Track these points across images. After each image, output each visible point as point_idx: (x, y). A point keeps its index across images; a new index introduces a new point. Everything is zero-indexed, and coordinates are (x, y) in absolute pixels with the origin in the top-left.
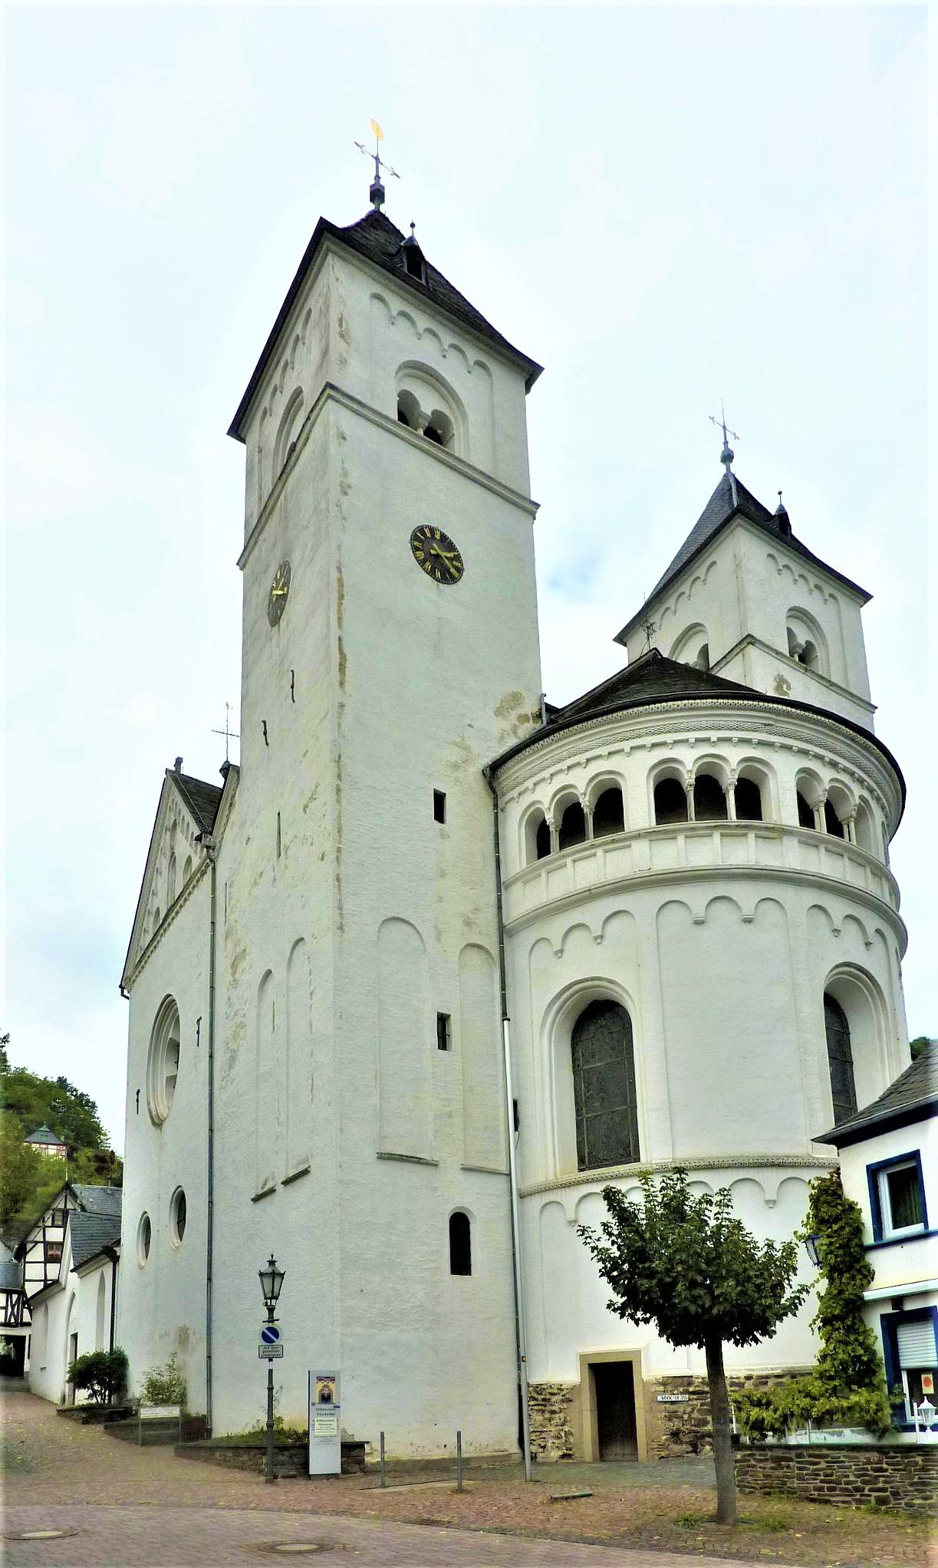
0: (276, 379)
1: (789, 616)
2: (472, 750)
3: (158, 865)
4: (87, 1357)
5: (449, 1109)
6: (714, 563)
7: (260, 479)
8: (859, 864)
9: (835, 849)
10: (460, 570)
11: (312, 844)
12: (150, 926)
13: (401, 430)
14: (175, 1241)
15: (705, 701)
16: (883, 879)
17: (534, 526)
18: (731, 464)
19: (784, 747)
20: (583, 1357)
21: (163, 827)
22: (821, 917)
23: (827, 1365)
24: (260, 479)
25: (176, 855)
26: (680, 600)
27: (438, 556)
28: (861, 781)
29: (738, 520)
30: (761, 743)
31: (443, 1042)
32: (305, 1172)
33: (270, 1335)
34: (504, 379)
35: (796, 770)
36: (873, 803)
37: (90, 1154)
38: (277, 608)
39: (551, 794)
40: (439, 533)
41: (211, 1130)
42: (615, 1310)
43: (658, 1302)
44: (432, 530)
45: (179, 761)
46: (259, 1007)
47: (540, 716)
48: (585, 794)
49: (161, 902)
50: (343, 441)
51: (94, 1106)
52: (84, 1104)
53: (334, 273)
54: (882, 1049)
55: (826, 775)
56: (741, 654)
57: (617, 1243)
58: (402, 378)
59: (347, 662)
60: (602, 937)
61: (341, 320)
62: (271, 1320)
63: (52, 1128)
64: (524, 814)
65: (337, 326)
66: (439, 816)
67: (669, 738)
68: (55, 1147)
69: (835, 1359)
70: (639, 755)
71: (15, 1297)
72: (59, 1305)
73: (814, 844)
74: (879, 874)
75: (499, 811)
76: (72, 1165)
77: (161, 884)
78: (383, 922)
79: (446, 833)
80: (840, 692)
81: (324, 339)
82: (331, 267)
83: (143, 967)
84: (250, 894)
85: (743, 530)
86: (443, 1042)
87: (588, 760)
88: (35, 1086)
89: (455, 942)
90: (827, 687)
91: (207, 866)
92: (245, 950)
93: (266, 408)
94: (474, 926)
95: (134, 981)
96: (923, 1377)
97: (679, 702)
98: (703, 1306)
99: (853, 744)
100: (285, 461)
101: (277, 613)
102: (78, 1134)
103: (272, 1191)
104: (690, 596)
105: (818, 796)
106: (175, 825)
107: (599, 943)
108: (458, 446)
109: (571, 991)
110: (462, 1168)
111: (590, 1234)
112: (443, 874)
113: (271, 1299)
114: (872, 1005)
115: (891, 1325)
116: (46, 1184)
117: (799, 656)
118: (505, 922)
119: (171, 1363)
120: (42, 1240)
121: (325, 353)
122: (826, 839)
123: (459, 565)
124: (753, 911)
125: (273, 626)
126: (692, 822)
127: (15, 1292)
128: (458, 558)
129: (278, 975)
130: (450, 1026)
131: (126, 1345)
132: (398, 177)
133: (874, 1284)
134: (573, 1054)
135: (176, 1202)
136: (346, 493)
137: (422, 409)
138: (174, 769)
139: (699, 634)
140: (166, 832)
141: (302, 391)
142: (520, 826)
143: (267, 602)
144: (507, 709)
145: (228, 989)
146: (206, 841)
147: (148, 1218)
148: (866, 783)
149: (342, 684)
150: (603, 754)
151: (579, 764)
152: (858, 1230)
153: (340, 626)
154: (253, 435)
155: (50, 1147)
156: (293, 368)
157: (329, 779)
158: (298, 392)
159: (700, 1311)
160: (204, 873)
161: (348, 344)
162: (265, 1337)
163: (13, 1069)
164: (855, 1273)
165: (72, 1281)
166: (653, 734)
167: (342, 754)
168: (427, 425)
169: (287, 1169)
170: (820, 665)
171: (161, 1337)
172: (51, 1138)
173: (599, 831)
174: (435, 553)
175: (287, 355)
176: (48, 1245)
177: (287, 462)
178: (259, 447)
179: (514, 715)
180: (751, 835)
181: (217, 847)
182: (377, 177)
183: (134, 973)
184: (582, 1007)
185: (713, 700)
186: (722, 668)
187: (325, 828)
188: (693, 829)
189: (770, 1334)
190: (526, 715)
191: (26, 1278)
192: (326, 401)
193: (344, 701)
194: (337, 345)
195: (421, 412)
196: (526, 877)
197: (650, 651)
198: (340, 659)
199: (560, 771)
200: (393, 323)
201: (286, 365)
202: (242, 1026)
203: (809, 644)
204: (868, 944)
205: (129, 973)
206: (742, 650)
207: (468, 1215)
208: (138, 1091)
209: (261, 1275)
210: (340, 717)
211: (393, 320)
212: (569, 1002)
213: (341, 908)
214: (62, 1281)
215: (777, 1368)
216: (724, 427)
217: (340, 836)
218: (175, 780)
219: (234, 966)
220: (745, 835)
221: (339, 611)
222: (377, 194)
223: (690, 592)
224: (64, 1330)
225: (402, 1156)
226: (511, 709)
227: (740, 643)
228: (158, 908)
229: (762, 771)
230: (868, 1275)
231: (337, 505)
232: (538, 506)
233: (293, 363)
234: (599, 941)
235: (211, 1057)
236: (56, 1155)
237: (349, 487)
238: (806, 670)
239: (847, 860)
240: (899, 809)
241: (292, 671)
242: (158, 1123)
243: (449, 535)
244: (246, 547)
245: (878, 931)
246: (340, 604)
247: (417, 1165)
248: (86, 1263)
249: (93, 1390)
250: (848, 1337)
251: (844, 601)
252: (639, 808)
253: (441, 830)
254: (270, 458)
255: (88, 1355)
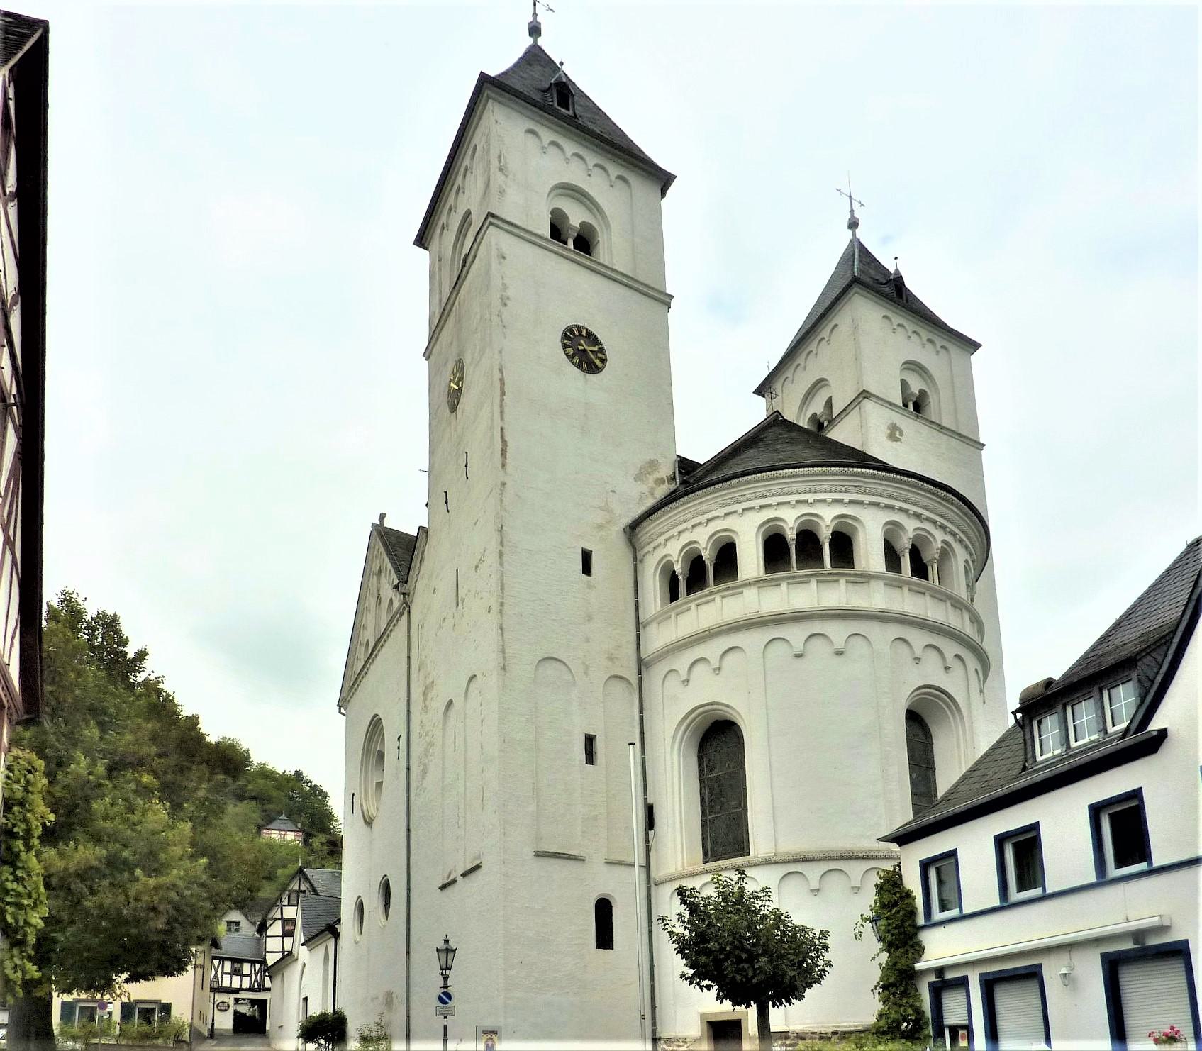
0: (451, 201)
1: (905, 369)
2: (615, 512)
3: (367, 604)
4: (314, 1017)
5: (595, 813)
6: (836, 326)
7: (440, 285)
8: (941, 600)
9: (916, 588)
10: (603, 361)
11: (482, 598)
12: (362, 654)
13: (556, 246)
14: (383, 920)
15: (802, 469)
16: (964, 610)
17: (669, 314)
18: (857, 230)
19: (872, 504)
20: (702, 1016)
21: (370, 572)
22: (902, 647)
23: (882, 1023)
24: (440, 285)
25: (382, 596)
26: (821, 345)
27: (585, 351)
28: (943, 527)
29: (855, 289)
30: (851, 502)
31: (590, 757)
32: (478, 867)
33: (445, 998)
34: (641, 188)
35: (884, 522)
36: (956, 546)
37: (323, 840)
38: (454, 399)
39: (680, 548)
40: (585, 331)
41: (409, 830)
42: (686, 979)
43: (713, 974)
44: (579, 328)
45: (383, 517)
46: (444, 729)
47: (673, 478)
48: (706, 549)
49: (370, 635)
50: (502, 260)
51: (326, 796)
52: (317, 794)
53: (493, 115)
54: (959, 755)
55: (910, 525)
56: (858, 407)
57: (688, 928)
58: (553, 198)
59: (508, 448)
60: (719, 669)
61: (500, 157)
62: (446, 986)
63: (289, 816)
64: (658, 564)
65: (497, 162)
66: (587, 569)
67: (774, 501)
68: (293, 833)
69: (888, 1018)
70: (750, 515)
71: (258, 966)
72: (293, 973)
73: (898, 585)
74: (959, 606)
75: (638, 562)
76: (307, 850)
77: (370, 619)
78: (539, 661)
79: (592, 584)
80: (950, 434)
81: (486, 173)
82: (491, 111)
83: (356, 690)
84: (436, 635)
85: (860, 297)
86: (590, 757)
87: (708, 520)
88: (274, 779)
89: (599, 675)
90: (938, 430)
91: (404, 609)
92: (433, 682)
93: (467, 166)
94: (615, 660)
95: (349, 701)
96: (961, 1032)
97: (781, 471)
98: (746, 977)
99: (934, 497)
100: (460, 269)
101: (454, 402)
102: (313, 821)
103: (454, 881)
104: (816, 354)
105: (904, 544)
106: (380, 571)
107: (718, 674)
108: (603, 253)
109: (690, 718)
110: (606, 862)
111: (668, 922)
112: (590, 618)
113: (445, 969)
114: (951, 719)
115: (937, 991)
116: (285, 867)
117: (913, 404)
118: (643, 656)
119: (379, 1021)
120: (280, 917)
121: (487, 185)
122: (909, 581)
123: (603, 356)
124: (843, 645)
125: (452, 412)
126: (794, 572)
127: (258, 962)
128: (602, 350)
129: (457, 704)
130: (595, 744)
131: (345, 1007)
132: (553, 11)
133: (925, 957)
134: (699, 765)
135: (384, 887)
136: (505, 305)
137: (571, 222)
138: (379, 523)
139: (823, 388)
140: (373, 578)
141: (470, 213)
142: (655, 575)
143: (446, 393)
144: (645, 474)
145: (421, 713)
146: (403, 588)
147: (361, 900)
148: (947, 529)
149: (503, 466)
150: (720, 515)
151: (700, 524)
152: (912, 913)
153: (502, 419)
154: (435, 244)
155: (288, 833)
156: (464, 193)
157: (493, 546)
158: (468, 214)
159: (744, 980)
160: (401, 615)
161: (507, 176)
162: (441, 999)
163: (255, 764)
164: (908, 948)
165: (303, 953)
166: (761, 497)
167: (504, 524)
168: (576, 235)
169: (465, 863)
170: (932, 411)
171: (373, 1000)
172: (290, 825)
173: (719, 578)
174: (583, 348)
175: (459, 181)
176: (285, 922)
177: (461, 270)
178: (439, 257)
179: (651, 478)
180: (842, 581)
181: (412, 593)
182: (535, 15)
183: (349, 694)
184: (708, 724)
185: (810, 469)
186: (842, 419)
187: (491, 586)
188: (794, 577)
189: (800, 998)
190: (662, 478)
191: (267, 950)
192: (488, 227)
193: (506, 481)
194: (498, 179)
195: (571, 225)
196: (661, 618)
197: (773, 413)
198: (502, 445)
199: (686, 529)
200: (545, 153)
201: (458, 189)
202: (431, 744)
203: (923, 393)
204: (947, 668)
205: (345, 694)
206: (859, 403)
207: (610, 899)
208: (353, 795)
209: (438, 950)
210: (502, 494)
211: (545, 150)
212: (693, 724)
213: (504, 652)
214: (295, 953)
215: (859, 1025)
216: (850, 197)
217: (503, 593)
218: (380, 534)
219: (425, 694)
220: (837, 581)
221: (501, 406)
222: (535, 30)
223: (817, 350)
224: (297, 994)
225: (556, 853)
226: (649, 474)
227: (857, 398)
228: (368, 641)
229: (853, 525)
230: (919, 950)
231: (498, 315)
232: (671, 297)
233: (464, 188)
234: (717, 672)
235: (408, 769)
236: (293, 841)
237: (508, 298)
238: (918, 417)
239: (929, 597)
240: (983, 543)
241: (467, 453)
242: (368, 822)
243: (595, 332)
244: (430, 342)
245: (957, 656)
246: (502, 400)
247: (569, 861)
248: (313, 938)
249: (319, 1044)
250: (901, 999)
251: (955, 351)
252: (750, 559)
253: (588, 582)
254: (448, 268)
255: (314, 1015)
